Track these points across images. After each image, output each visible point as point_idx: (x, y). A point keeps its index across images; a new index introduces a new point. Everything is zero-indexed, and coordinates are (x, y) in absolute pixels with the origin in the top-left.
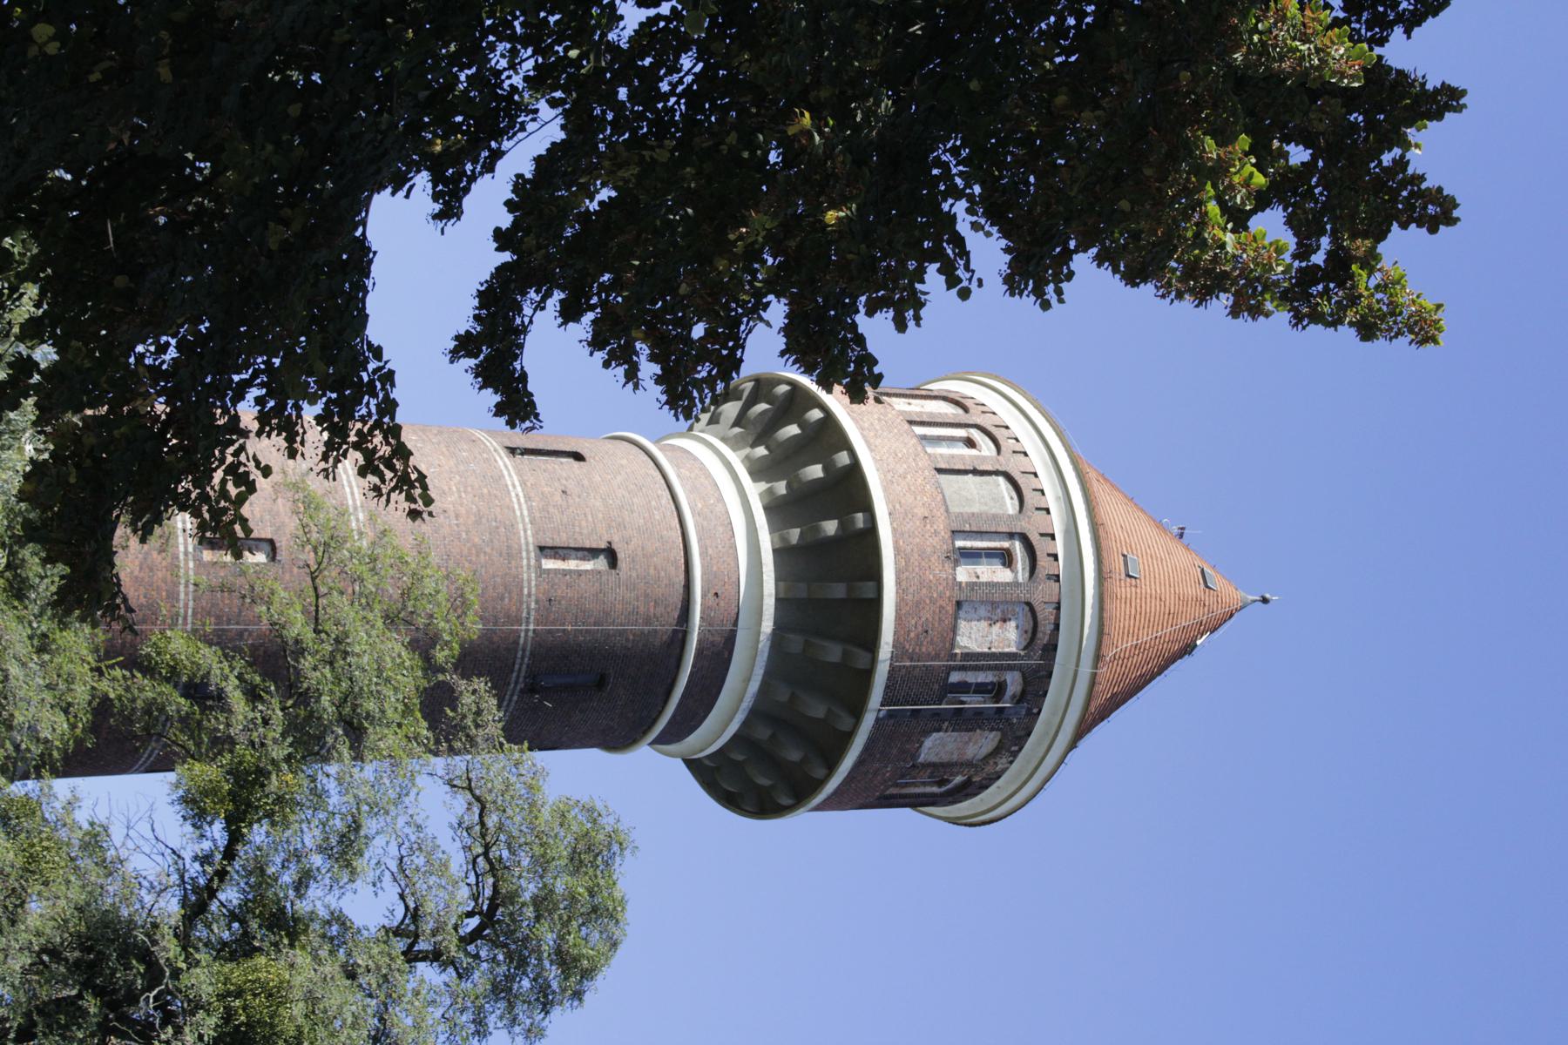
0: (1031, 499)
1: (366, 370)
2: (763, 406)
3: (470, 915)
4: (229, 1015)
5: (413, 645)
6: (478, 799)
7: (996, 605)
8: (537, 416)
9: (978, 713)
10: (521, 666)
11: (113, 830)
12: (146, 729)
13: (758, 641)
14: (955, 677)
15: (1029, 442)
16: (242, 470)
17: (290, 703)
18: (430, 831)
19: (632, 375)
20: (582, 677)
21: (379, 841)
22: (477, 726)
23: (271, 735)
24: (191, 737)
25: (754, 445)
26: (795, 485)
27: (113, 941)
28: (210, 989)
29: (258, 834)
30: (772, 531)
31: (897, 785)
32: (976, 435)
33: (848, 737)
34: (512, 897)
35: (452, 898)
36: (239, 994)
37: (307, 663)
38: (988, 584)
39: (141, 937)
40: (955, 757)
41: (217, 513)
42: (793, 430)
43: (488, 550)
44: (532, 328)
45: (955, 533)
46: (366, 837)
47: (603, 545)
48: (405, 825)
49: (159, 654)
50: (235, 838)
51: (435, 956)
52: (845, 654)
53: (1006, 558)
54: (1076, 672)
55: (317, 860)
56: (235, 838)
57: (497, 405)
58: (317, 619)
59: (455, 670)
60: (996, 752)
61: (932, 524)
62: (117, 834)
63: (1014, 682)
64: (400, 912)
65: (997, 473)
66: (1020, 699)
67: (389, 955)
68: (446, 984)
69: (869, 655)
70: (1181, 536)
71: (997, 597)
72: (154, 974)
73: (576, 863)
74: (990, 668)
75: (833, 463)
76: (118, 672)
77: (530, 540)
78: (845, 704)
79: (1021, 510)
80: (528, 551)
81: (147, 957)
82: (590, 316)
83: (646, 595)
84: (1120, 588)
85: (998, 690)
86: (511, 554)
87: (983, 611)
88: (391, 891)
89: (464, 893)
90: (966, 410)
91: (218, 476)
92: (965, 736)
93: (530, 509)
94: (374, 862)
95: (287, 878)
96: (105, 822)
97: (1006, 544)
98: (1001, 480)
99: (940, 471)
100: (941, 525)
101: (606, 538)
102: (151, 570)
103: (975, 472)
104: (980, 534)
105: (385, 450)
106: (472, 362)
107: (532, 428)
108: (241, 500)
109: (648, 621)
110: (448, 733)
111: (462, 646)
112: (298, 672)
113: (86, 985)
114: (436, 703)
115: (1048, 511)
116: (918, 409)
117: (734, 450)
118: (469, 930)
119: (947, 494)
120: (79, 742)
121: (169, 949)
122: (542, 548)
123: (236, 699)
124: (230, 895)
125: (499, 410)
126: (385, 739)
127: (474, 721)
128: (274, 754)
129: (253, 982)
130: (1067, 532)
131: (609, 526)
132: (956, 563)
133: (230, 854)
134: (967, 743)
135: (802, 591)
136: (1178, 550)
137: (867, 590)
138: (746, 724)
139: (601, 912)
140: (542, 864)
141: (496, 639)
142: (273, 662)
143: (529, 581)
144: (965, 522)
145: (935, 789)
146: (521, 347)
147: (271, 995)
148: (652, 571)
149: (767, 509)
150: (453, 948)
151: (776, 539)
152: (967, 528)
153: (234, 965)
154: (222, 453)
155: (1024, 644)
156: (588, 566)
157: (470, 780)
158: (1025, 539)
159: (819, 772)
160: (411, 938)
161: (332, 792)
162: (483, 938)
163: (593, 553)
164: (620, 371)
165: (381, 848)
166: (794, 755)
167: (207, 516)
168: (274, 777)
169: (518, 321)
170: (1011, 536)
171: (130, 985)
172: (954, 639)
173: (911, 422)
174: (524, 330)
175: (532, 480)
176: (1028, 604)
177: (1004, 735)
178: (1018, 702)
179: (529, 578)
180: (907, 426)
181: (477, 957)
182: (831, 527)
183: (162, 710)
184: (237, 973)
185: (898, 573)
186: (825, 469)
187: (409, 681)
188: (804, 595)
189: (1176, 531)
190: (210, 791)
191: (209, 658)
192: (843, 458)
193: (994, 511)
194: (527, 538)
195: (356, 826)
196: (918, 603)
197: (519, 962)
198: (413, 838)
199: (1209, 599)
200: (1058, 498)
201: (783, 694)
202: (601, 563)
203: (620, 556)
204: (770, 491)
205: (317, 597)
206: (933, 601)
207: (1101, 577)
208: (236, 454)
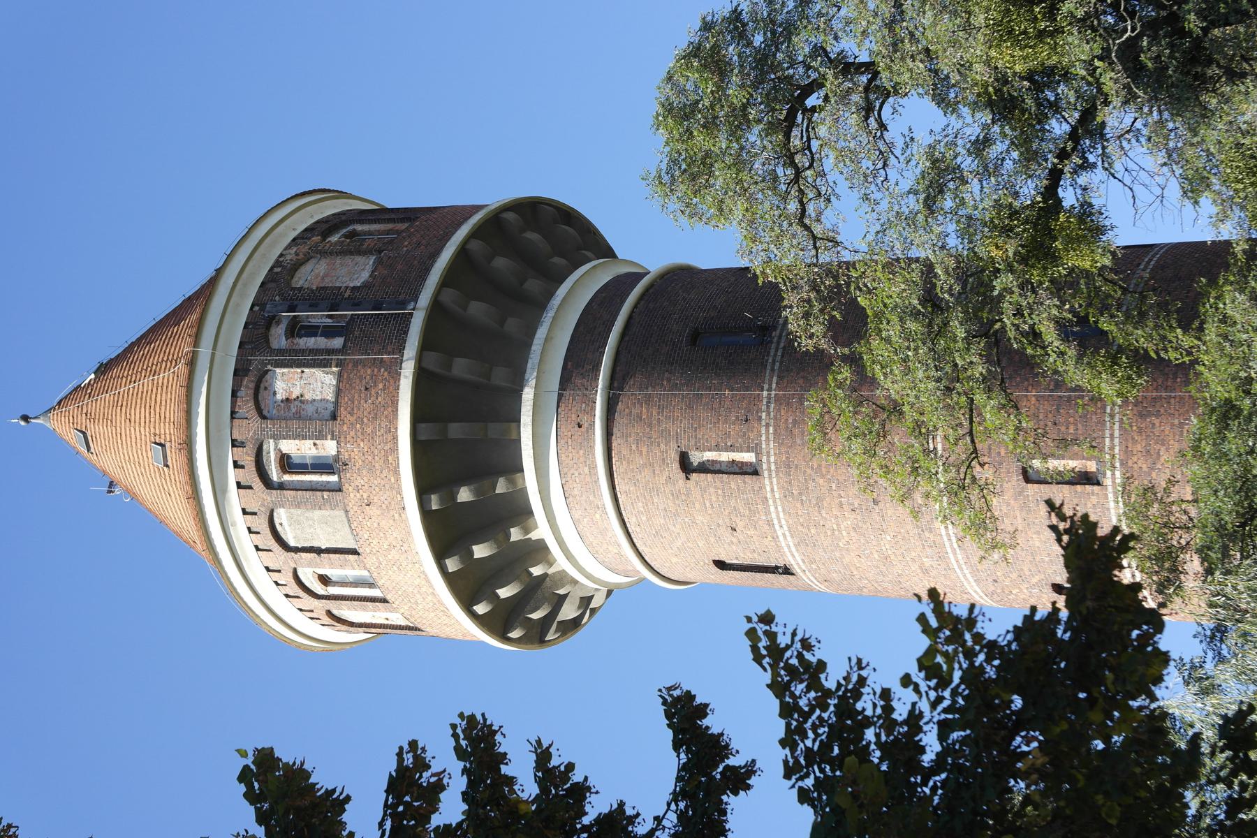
0: (261, 524)
1: (816, 778)
2: (535, 616)
3: (813, 109)
4: (1051, 13)
5: (873, 382)
6: (807, 228)
7: (297, 416)
8: (665, 702)
9: (314, 307)
10: (775, 353)
11: (1179, 193)
12: (1143, 298)
13: (538, 378)
14: (338, 342)
15: (263, 582)
16: (933, 683)
17: (997, 326)
18: (856, 194)
19: (543, 756)
20: (707, 344)
21: (906, 185)
22: (809, 301)
23: (1015, 297)
24: (1097, 289)
25: (545, 575)
26: (501, 537)
27: (1173, 85)
28: (1070, 39)
29: (1029, 190)
30: (524, 491)
31: (398, 232)
32: (319, 588)
33: (445, 282)
34: (772, 128)
35: (834, 127)
36: (1041, 34)
37: (980, 370)
38: (304, 438)
39: (1140, 93)
40: (338, 260)
41: (956, 638)
42: (504, 593)
43: (809, 471)
44: (668, 798)
45: (338, 489)
46: (916, 193)
47: (694, 476)
48: (877, 199)
49: (1129, 377)
50: (1051, 191)
51: (847, 68)
52: (449, 367)
53: (286, 463)
54: (214, 348)
55: (968, 163)
56: (1051, 191)
57: (705, 715)
58: (971, 410)
59: (831, 356)
60: (297, 266)
61: (361, 499)
62: (1174, 189)
63: (278, 336)
64: (886, 113)
65: (297, 550)
66: (271, 321)
67: (891, 72)
68: (836, 38)
69: (424, 365)
70: (111, 484)
71: (295, 424)
72: (1129, 56)
73: (707, 161)
74: (302, 352)
75: (462, 561)
76: (1172, 355)
77: (767, 481)
78: (448, 319)
79: (272, 512)
80: (769, 470)
81: (1134, 69)
82: (586, 820)
83: (650, 425)
84: (170, 433)
85: (295, 329)
86: (786, 467)
87: (310, 409)
88: (894, 133)
89: (822, 131)
90: (329, 613)
91: (957, 675)
92: (328, 283)
93: (768, 513)
94: (913, 163)
95: (999, 147)
96: (1186, 202)
97: (287, 477)
98: (292, 543)
99: (354, 552)
100: (352, 497)
101: (691, 484)
102: (1148, 452)
103: (318, 551)
104: (313, 488)
105: (799, 688)
106: (732, 761)
107: (669, 689)
108: (931, 652)
109: (648, 399)
110: (839, 293)
111: (826, 380)
112: (989, 361)
113: (1197, 42)
114: (851, 324)
115: (245, 512)
116: (377, 614)
117: (564, 571)
118: (815, 95)
119: (347, 529)
120: (1213, 282)
121: (1111, 80)
122: (756, 473)
123: (1050, 334)
124: (1058, 128)
125: (702, 710)
126: (899, 290)
127: (811, 306)
128: (1011, 277)
129: (1026, 46)
130: (225, 490)
131: (688, 495)
132: (337, 458)
133: (1055, 176)
134: (326, 275)
135: (494, 430)
136: (114, 470)
137: (427, 432)
138: (551, 294)
139: (679, 113)
140: (740, 163)
141: (801, 381)
142: (1012, 365)
143: (768, 439)
144: (328, 501)
145: (359, 228)
146: (679, 779)
147: (1010, 33)
148: (644, 449)
149: (530, 513)
150: (830, 76)
151: (520, 482)
152: (326, 494)
153: (1048, 63)
154: (954, 702)
155: (268, 377)
156: (709, 455)
157: (815, 247)
159: (475, 245)
160: (873, 90)
161: (953, 235)
162: (799, 87)
163: (704, 468)
164: (554, 762)
165: (906, 176)
166: (500, 263)
167: (968, 636)
168: (1011, 254)
169: (682, 805)
170: (281, 487)
171: (1154, 39)
172: (339, 381)
173: (384, 601)
174: (676, 797)
175: (766, 541)
176: (263, 417)
177: (288, 283)
178: (274, 317)
179: (768, 444)
180: (388, 598)
181: (808, 67)
182: (464, 495)
183: (1128, 316)
184: (1044, 55)
185: (395, 449)
186: (472, 553)
187: (877, 350)
188: (491, 426)
189: (117, 491)
190: (1073, 241)
191: (1077, 375)
192: (452, 565)
193: (299, 512)
194: (770, 483)
195: (930, 205)
196: (375, 418)
197: (763, 62)
198: (873, 187)
199: (82, 421)
200: (234, 524)
201: (512, 325)
202: (696, 458)
203: (677, 465)
204: (527, 531)
205: (971, 433)
206: (360, 420)
207: (188, 445)
208: (940, 699)
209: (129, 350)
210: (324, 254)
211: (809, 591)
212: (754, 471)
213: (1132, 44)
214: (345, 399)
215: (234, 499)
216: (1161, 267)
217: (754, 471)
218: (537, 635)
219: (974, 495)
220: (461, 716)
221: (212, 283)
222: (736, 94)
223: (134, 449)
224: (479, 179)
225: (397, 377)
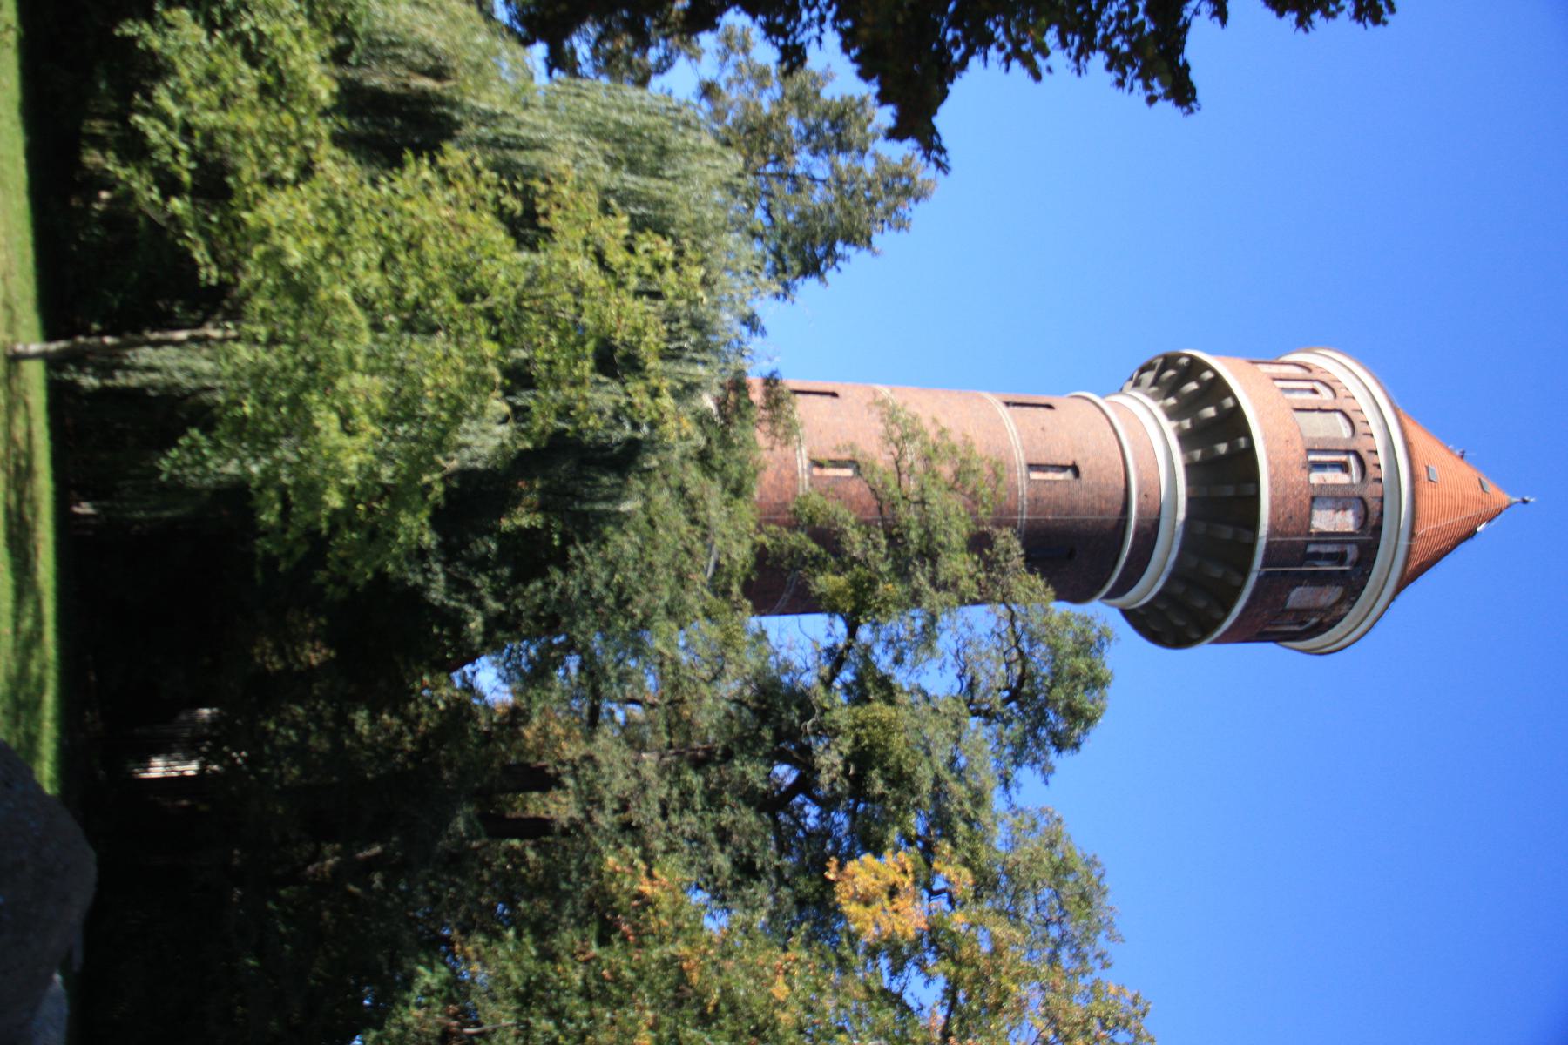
0: (1360, 427)
7: (1338, 499)
14: (1312, 549)
25: (1166, 397)
29: (864, 634)
33: (1238, 591)
35: (994, 675)
36: (863, 726)
40: (1311, 605)
45: (1310, 451)
47: (1070, 463)
53: (1344, 467)
63: (1352, 552)
65: (1335, 410)
66: (1356, 564)
71: (1339, 493)
84: (1425, 488)
85: (1340, 558)
87: (1329, 503)
88: (952, 674)
92: (1318, 589)
97: (1343, 458)
98: (1338, 415)
100: (1299, 447)
103: (1320, 410)
109: (1101, 512)
132: (1310, 471)
136: (1462, 465)
137: (1250, 490)
138: (1167, 583)
145: (1296, 628)
156: (1060, 476)
158: (1356, 453)
159: (1220, 615)
163: (1063, 468)
166: (1201, 603)
170: (1347, 452)
179: (1022, 484)
182: (1222, 448)
184: (861, 712)
185: (1272, 477)
189: (1458, 452)
192: (1229, 402)
194: (1020, 458)
199: (1485, 499)
202: (1069, 475)
203: (1082, 470)
209: (1454, 547)
210: (1321, 610)
211: (992, 390)
212: (1032, 467)
213: (804, 718)
214: (1306, 510)
215: (1379, 443)
216: (776, 600)
217: (1032, 467)
218: (1169, 361)
219: (897, 434)
220: (1385, 23)
221: (1400, 588)
222: (1059, 693)
223: (1450, 482)
224: (1213, 662)
225: (1272, 527)
